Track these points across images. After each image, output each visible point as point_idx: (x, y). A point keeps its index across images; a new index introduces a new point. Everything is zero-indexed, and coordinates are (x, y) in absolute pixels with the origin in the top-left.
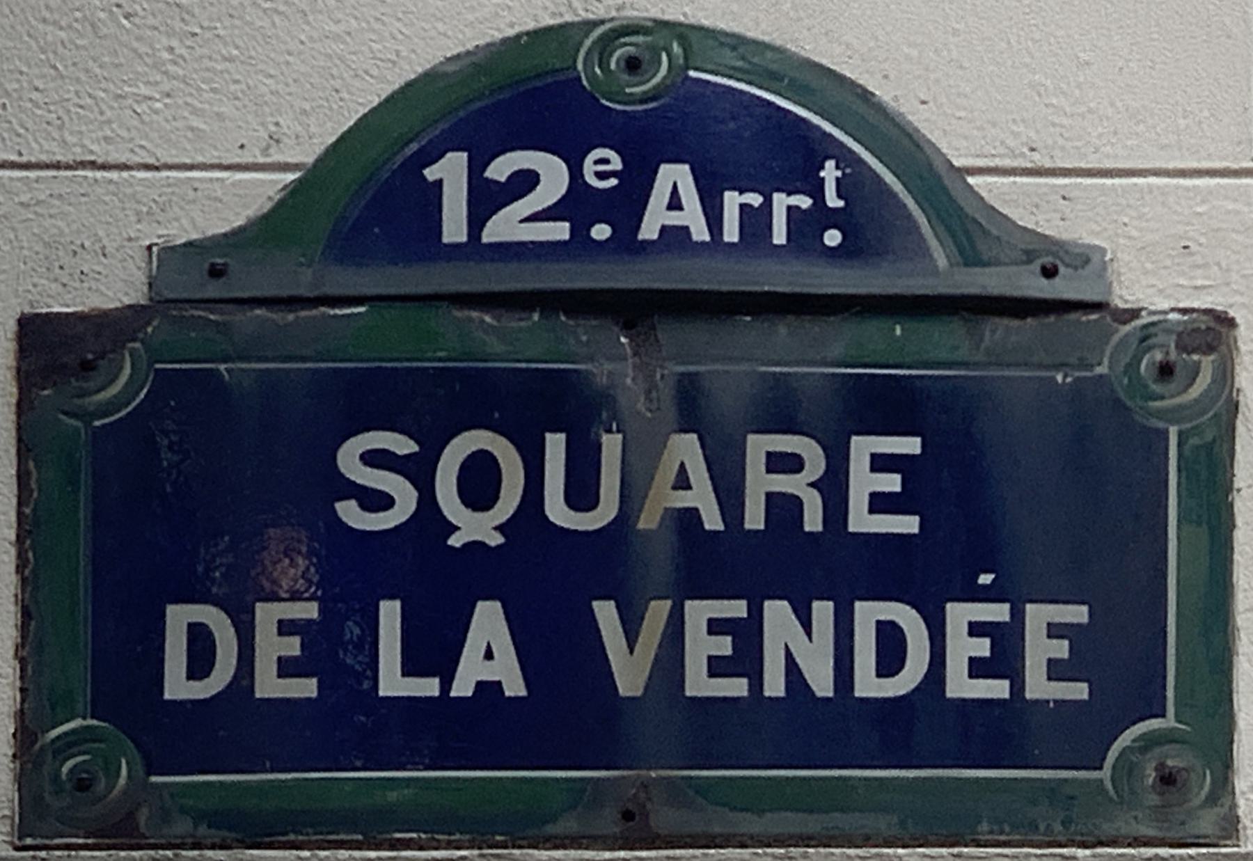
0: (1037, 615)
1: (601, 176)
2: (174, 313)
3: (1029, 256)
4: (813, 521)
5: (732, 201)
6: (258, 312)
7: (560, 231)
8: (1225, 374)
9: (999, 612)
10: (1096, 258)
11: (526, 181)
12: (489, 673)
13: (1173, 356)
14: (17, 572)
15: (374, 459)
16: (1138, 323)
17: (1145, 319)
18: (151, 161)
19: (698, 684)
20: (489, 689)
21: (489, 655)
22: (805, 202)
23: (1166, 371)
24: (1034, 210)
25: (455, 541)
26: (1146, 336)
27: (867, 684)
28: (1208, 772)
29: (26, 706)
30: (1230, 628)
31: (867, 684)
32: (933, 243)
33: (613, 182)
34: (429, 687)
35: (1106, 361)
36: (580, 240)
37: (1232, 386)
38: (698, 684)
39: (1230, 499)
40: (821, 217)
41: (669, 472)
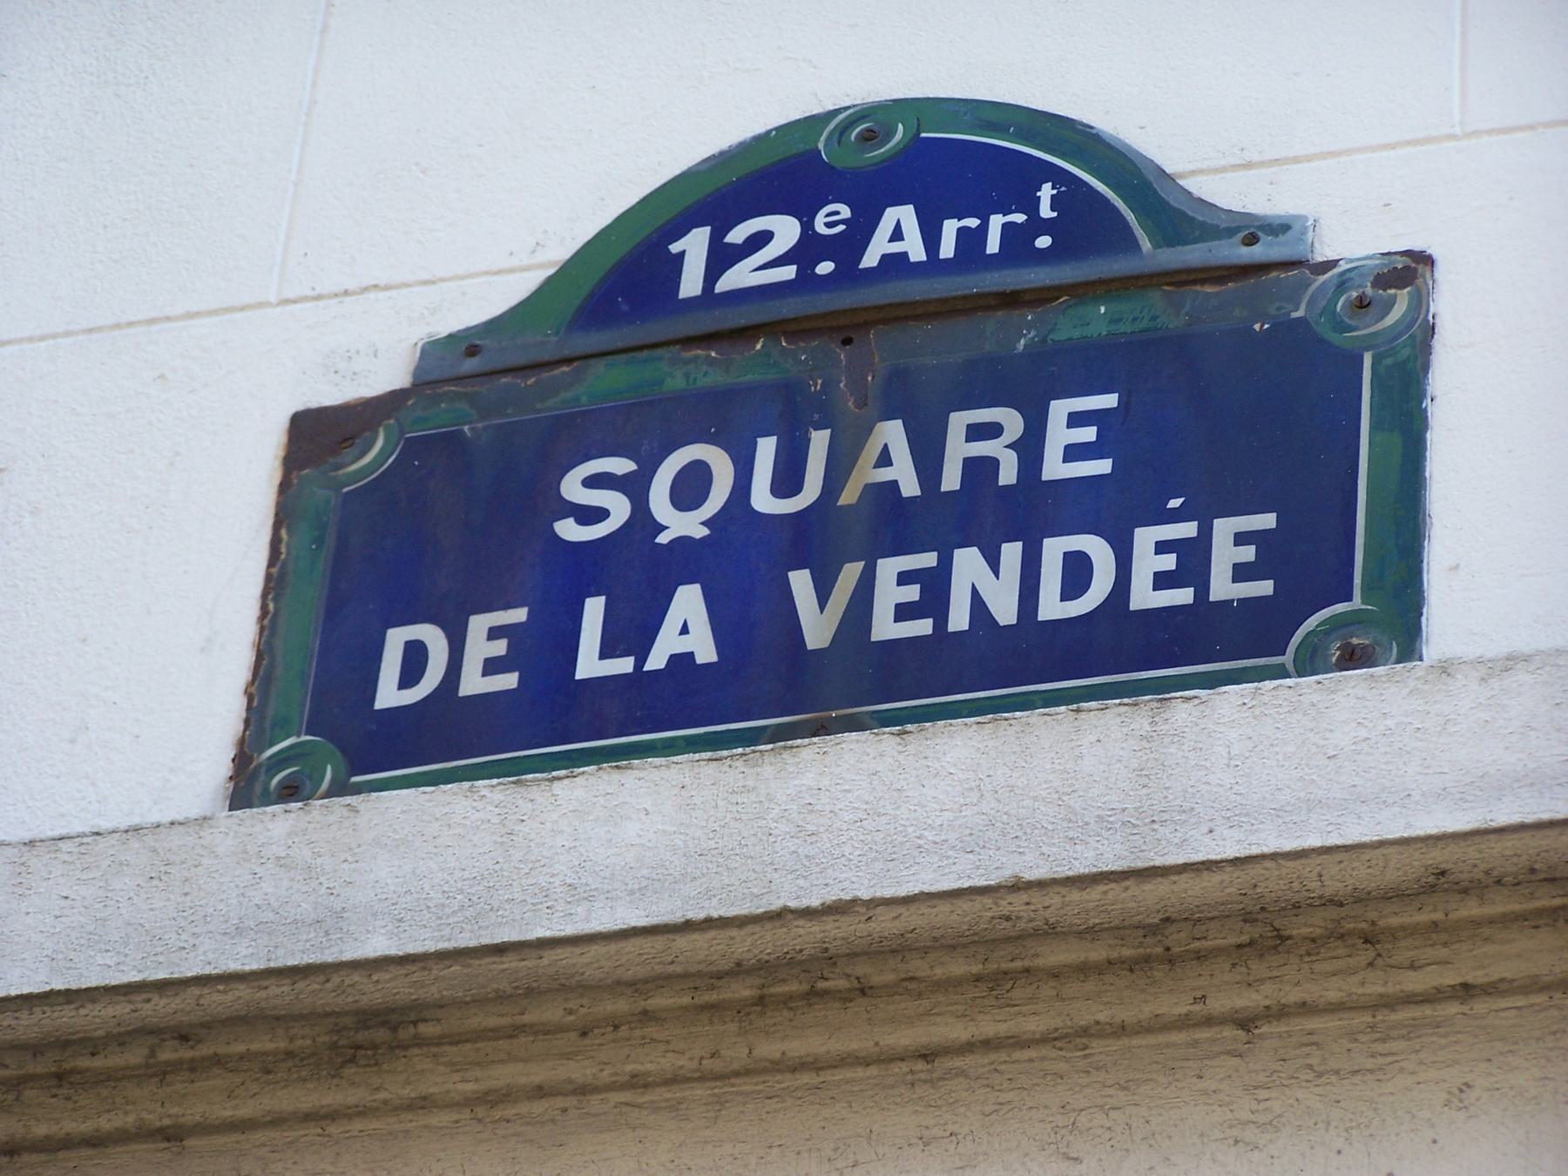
0: (1225, 528)
1: (829, 225)
2: (429, 392)
3: (1231, 232)
4: (1008, 474)
5: (950, 228)
6: (504, 380)
7: (788, 272)
8: (1420, 302)
9: (1188, 529)
10: (1297, 227)
11: (763, 238)
12: (681, 645)
13: (1369, 291)
14: (258, 623)
15: (592, 482)
16: (1336, 271)
17: (1343, 266)
18: (426, 276)
19: (885, 627)
20: (684, 662)
21: (685, 630)
22: (1019, 218)
23: (1362, 304)
24: (642, 833)
25: (663, 539)
26: (1343, 284)
27: (1051, 607)
28: (1394, 644)
29: (248, 733)
30: (1421, 516)
31: (1051, 607)
32: (1139, 233)
33: (842, 227)
34: (625, 665)
35: (1303, 306)
36: (806, 279)
37: (1428, 311)
38: (885, 627)
39: (1424, 406)
40: (1037, 226)
41: (872, 451)
